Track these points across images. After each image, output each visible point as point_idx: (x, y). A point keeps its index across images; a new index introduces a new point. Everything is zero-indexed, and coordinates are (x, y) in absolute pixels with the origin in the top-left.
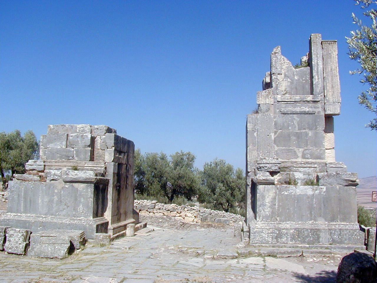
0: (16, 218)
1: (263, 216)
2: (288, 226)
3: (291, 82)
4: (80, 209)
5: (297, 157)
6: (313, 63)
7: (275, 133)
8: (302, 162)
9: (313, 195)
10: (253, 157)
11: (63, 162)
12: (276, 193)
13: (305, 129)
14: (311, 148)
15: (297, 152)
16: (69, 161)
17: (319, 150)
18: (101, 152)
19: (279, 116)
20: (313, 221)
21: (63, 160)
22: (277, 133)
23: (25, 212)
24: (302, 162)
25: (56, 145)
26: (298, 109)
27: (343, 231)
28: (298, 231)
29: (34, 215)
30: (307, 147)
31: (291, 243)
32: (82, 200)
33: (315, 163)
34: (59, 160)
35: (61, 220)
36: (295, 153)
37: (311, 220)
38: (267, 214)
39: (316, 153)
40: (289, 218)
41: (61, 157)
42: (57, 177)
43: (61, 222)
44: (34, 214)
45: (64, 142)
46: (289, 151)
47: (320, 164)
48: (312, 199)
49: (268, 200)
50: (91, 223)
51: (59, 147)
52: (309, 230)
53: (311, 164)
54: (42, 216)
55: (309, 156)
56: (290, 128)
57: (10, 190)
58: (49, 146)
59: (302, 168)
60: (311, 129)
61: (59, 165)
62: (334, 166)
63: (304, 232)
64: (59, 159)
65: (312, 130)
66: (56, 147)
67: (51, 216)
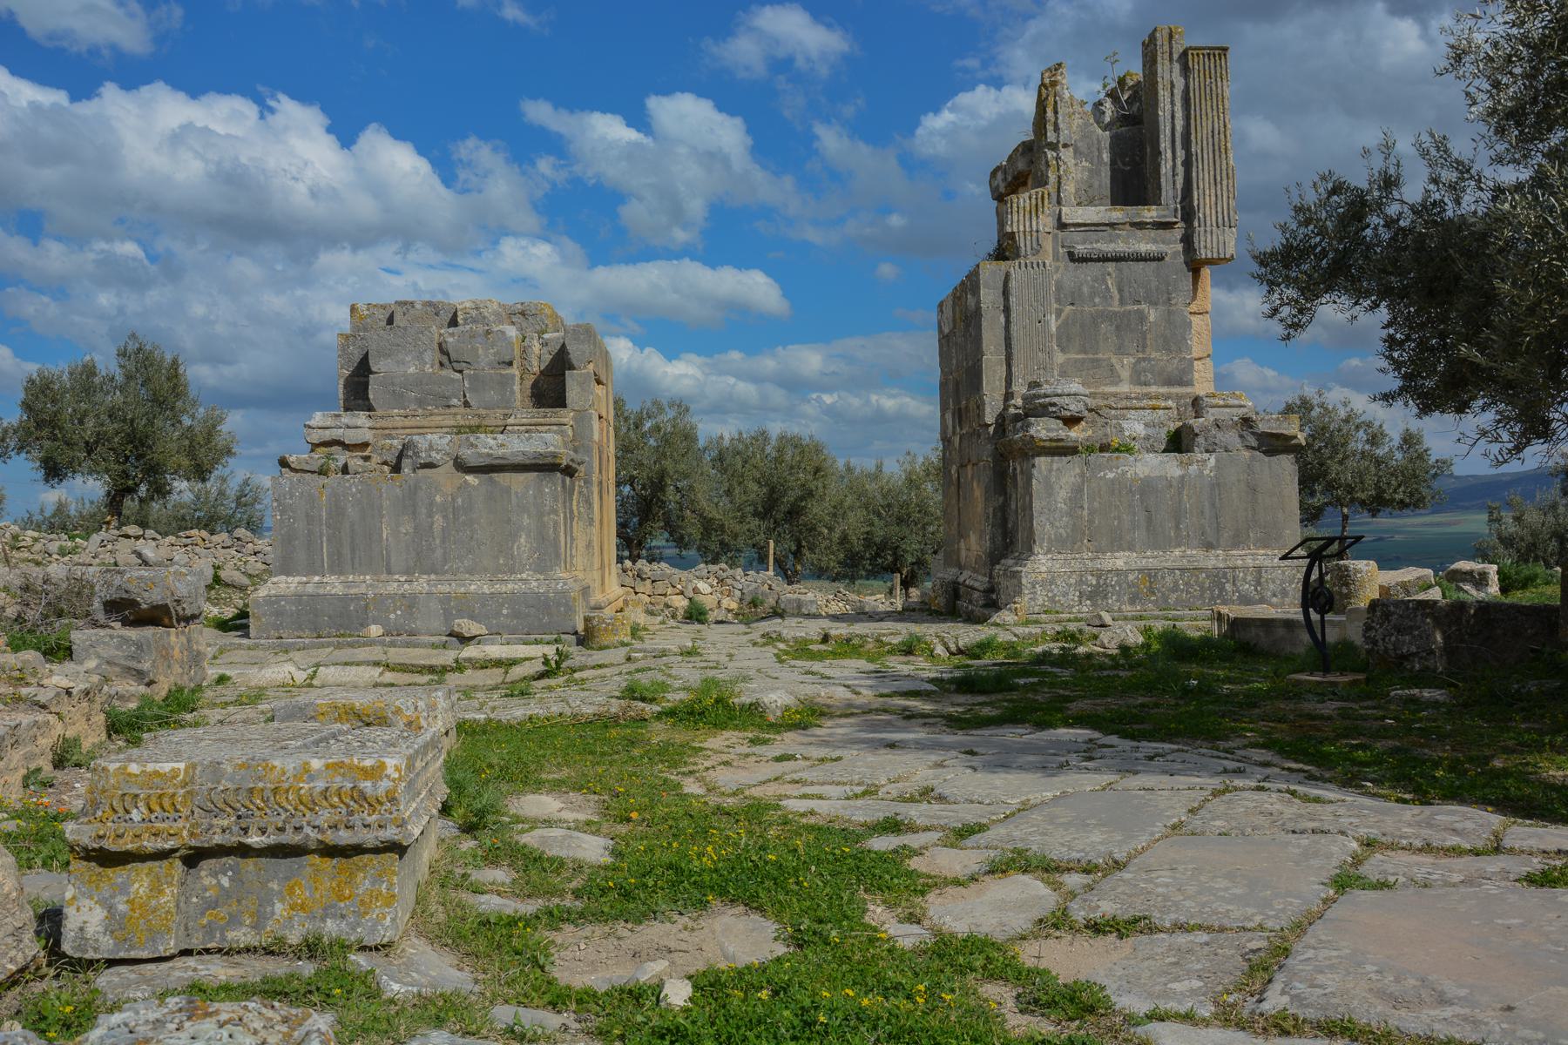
0: (310, 589)
1: (1049, 538)
2: (1120, 564)
3: (1090, 171)
4: (519, 548)
6: (1160, 113)
7: (1059, 313)
9: (1182, 477)
12: (1082, 475)
13: (1139, 302)
15: (1118, 367)
16: (448, 411)
17: (1176, 361)
22: (1063, 315)
23: (337, 568)
26: (1120, 247)
30: (1143, 352)
31: (1129, 608)
32: (526, 521)
33: (1167, 397)
35: (464, 585)
39: (1170, 369)
40: (1118, 543)
41: (421, 403)
43: (462, 590)
45: (429, 352)
46: (1096, 363)
47: (1179, 397)
49: (1062, 494)
50: (559, 587)
51: (412, 370)
53: (1157, 398)
54: (397, 577)
55: (1150, 376)
56: (1097, 300)
59: (1133, 412)
60: (1154, 303)
61: (419, 424)
62: (1221, 402)
63: (1163, 578)
65: (1156, 304)
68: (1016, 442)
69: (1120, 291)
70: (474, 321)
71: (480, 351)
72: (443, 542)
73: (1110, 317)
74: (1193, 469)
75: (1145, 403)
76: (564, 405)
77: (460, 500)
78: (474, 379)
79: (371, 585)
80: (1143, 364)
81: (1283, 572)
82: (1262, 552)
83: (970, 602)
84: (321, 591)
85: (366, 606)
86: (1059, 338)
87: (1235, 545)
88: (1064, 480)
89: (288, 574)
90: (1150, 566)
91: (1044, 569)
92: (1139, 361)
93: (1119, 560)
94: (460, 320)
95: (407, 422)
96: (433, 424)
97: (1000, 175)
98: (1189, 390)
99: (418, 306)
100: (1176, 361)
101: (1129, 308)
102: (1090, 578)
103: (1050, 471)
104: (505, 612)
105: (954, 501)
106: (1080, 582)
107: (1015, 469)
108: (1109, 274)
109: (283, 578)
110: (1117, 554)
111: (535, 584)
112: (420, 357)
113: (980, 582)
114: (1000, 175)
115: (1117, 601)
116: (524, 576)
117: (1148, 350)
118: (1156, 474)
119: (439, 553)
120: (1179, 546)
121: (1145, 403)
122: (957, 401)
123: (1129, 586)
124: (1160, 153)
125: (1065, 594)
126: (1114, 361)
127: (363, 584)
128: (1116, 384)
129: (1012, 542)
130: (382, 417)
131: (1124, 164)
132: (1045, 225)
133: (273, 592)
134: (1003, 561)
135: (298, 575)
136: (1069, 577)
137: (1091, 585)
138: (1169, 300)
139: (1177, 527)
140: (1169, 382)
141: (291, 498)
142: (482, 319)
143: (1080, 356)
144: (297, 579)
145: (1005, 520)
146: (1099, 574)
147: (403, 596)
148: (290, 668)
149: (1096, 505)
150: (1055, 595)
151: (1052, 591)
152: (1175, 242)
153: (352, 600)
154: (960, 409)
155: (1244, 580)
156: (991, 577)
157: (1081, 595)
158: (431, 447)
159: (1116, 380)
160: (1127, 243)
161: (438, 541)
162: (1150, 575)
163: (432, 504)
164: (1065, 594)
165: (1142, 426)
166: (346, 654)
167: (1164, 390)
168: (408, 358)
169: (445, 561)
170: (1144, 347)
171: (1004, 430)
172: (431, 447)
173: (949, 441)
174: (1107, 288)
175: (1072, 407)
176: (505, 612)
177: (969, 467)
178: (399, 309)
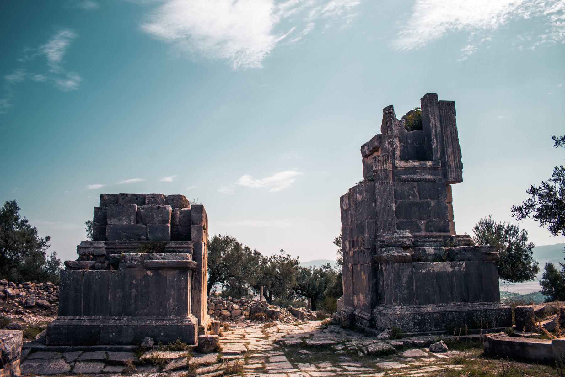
0: (74, 322)
2: (430, 309)
4: (169, 304)
5: (420, 230)
8: (426, 236)
9: (453, 271)
10: (372, 231)
11: (132, 243)
12: (412, 271)
13: (427, 199)
14: (434, 220)
17: (442, 222)
18: (180, 229)
19: (398, 184)
20: (455, 302)
21: (132, 240)
22: (397, 203)
23: (87, 313)
24: (426, 235)
25: (120, 220)
27: (489, 312)
28: (442, 315)
29: (101, 317)
30: (430, 218)
32: (173, 292)
33: (440, 237)
34: (125, 241)
35: (144, 321)
36: (417, 226)
37: (453, 301)
38: (404, 297)
39: (440, 226)
40: (428, 301)
42: (135, 263)
43: (143, 324)
44: (101, 316)
48: (451, 276)
51: (125, 223)
52: (453, 313)
55: (433, 228)
56: (411, 197)
57: (63, 284)
58: (111, 221)
63: (448, 315)
64: (126, 239)
66: (121, 222)
67: (127, 317)
68: (383, 257)
69: (419, 194)
70: (153, 203)
71: (155, 216)
72: (135, 301)
73: (416, 204)
74: (457, 268)
75: (431, 239)
76: (190, 240)
77: (144, 282)
79: (102, 321)
80: (430, 223)
81: (496, 312)
82: (486, 303)
83: (362, 324)
84: (79, 324)
85: (100, 330)
86: (396, 213)
87: (475, 300)
88: (405, 274)
89: (65, 315)
90: (442, 310)
91: (398, 313)
92: (428, 222)
93: (429, 308)
94: (146, 202)
95: (122, 246)
96: (133, 247)
97: (366, 148)
98: (448, 234)
99: (129, 196)
100: (442, 222)
101: (423, 200)
102: (418, 316)
103: (399, 269)
104: (162, 334)
105: (350, 278)
106: (414, 318)
107: (382, 268)
108: (415, 187)
109: (63, 317)
110: (428, 305)
111: (176, 321)
112: (129, 218)
113: (366, 316)
114: (366, 148)
115: (430, 326)
116: (171, 317)
117: (432, 217)
118: (442, 270)
119: (133, 306)
120: (453, 301)
121: (431, 239)
122: (352, 237)
123: (434, 320)
124: (431, 140)
125: (408, 324)
126: (418, 222)
127: (98, 321)
128: (420, 232)
129: (380, 299)
130: (111, 244)
131: (417, 144)
132: (389, 168)
133: (58, 323)
134: (377, 307)
135: (69, 315)
136: (410, 316)
137: (419, 319)
138: (439, 197)
139: (452, 292)
140: (440, 231)
141: (68, 281)
142: (155, 202)
143: (404, 220)
144: (69, 317)
145: (377, 289)
146: (421, 314)
147: (116, 326)
148: (62, 362)
149: (418, 284)
150: (404, 324)
151: (402, 322)
152: (439, 175)
153: (93, 328)
154: (353, 241)
155: (480, 315)
156: (372, 314)
157: (415, 324)
158: (132, 259)
159: (420, 230)
160: (421, 175)
161: (133, 301)
162: (442, 314)
163: (131, 284)
164: (408, 324)
165: (433, 250)
166: (88, 355)
167: (438, 234)
170: (430, 216)
171: (375, 252)
172: (132, 259)
173: (347, 253)
174: (414, 193)
175: (407, 243)
176: (162, 334)
177: (359, 266)
178: (121, 197)
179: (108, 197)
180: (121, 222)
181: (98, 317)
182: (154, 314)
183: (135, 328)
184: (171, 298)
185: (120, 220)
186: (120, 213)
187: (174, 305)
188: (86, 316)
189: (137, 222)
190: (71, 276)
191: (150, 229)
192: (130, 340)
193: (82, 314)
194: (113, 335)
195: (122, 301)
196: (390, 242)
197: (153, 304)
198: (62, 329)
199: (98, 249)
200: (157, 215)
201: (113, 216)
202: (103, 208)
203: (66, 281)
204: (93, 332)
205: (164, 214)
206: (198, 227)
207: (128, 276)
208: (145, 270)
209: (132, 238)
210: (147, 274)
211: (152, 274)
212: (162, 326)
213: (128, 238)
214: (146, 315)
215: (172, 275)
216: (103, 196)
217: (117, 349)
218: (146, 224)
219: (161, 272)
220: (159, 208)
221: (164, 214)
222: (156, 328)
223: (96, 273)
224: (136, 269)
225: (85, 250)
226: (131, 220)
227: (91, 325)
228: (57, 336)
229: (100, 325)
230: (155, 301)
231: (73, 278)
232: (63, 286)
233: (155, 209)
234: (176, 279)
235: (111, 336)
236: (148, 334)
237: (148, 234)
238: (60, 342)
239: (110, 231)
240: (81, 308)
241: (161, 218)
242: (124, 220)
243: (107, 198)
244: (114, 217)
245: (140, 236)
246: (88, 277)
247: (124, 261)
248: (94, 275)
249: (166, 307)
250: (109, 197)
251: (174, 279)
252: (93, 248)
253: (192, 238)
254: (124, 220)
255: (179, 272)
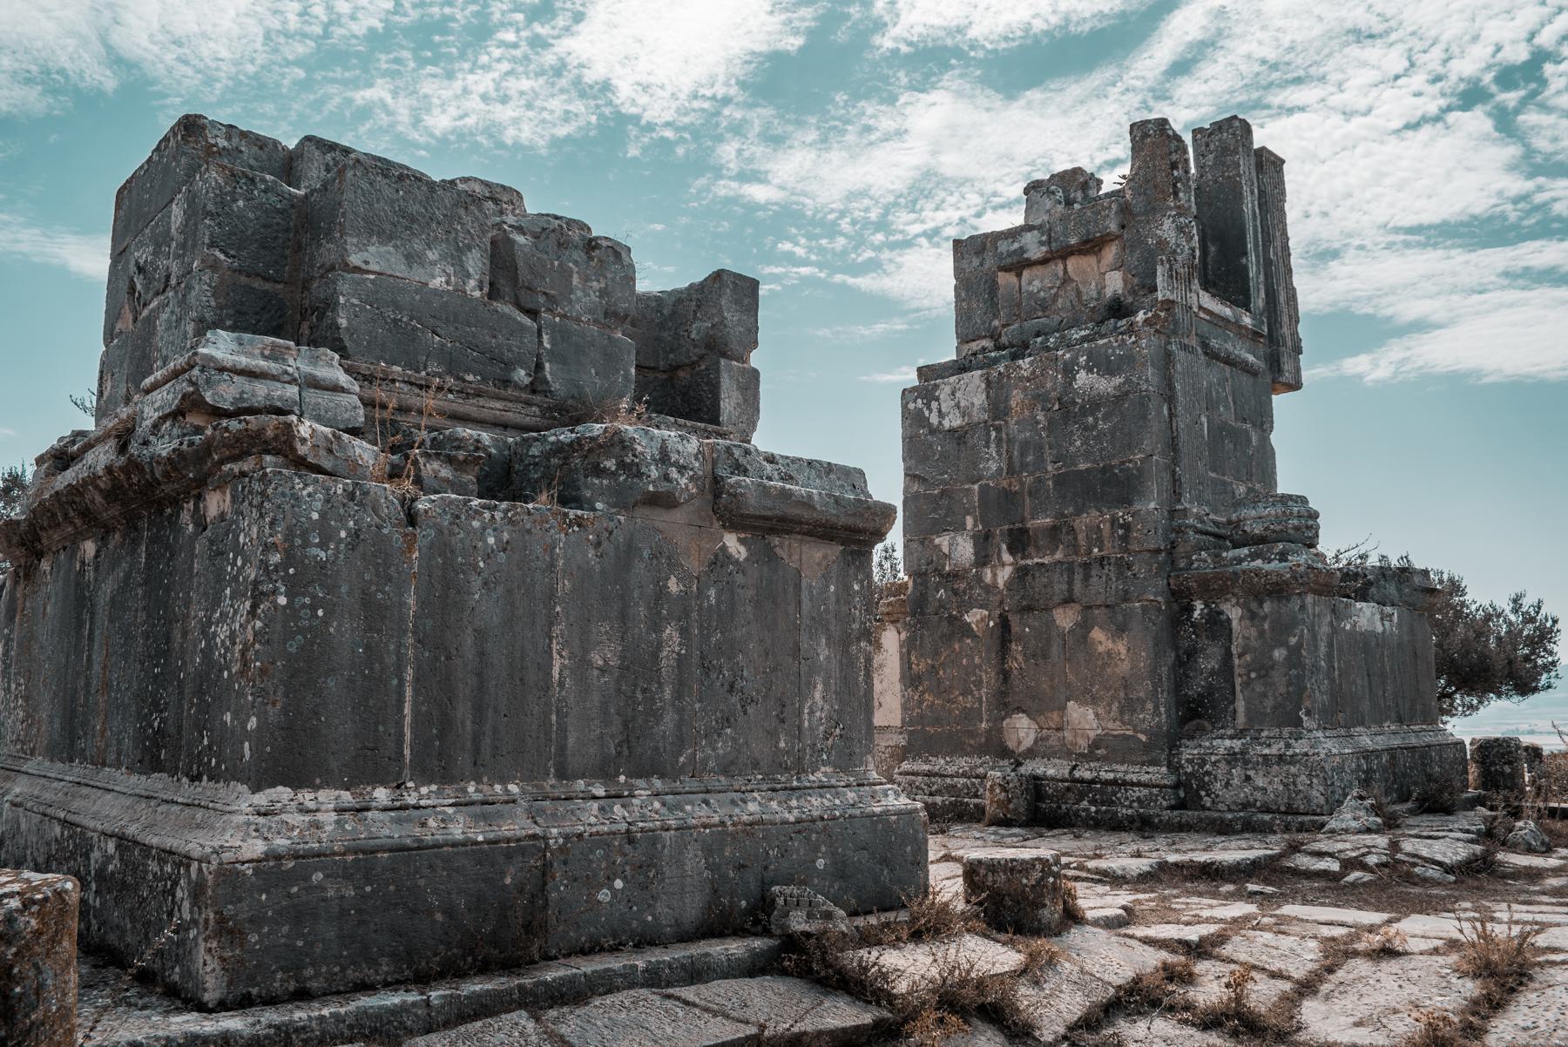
0: (384, 828)
44: (511, 779)
51: (438, 282)
57: (284, 565)
66: (418, 274)
71: (575, 280)
72: (678, 695)
78: (561, 334)
85: (545, 870)
109: (283, 793)
112: (456, 257)
119: (669, 720)
135: (326, 784)
141: (323, 545)
153: (509, 855)
161: (668, 692)
163: (661, 593)
168: (432, 255)
169: (680, 743)
172: (664, 457)
176: (820, 863)
179: (229, 138)
180: (418, 274)
181: (498, 788)
182: (756, 765)
183: (717, 840)
184: (819, 679)
185: (411, 259)
186: (413, 220)
187: (829, 718)
188: (430, 783)
189: (494, 293)
190: (342, 520)
191: (553, 341)
192: (692, 908)
193: (407, 772)
194: (614, 892)
195: (619, 691)
196: (1278, 528)
197: (750, 710)
198: (318, 877)
199: (327, 395)
200: (586, 279)
201: (377, 230)
202: (263, 180)
203: (306, 544)
204: (508, 881)
205: (613, 280)
206: (743, 375)
207: (646, 554)
208: (717, 524)
209: (468, 371)
210: (724, 548)
211: (742, 549)
212: (820, 824)
213: (453, 366)
214: (725, 771)
215: (819, 564)
216: (204, 127)
217: (683, 966)
218: (533, 313)
219: (781, 546)
220: (594, 248)
221: (613, 280)
222: (799, 832)
223: (487, 515)
224: (678, 516)
225: (247, 387)
226: (469, 276)
227: (496, 842)
228: (285, 929)
229: (545, 838)
230: (758, 692)
231: (355, 534)
232: (287, 579)
233: (576, 247)
234: (832, 588)
235: (604, 896)
236: (766, 868)
237: (547, 365)
238: (309, 972)
239: (363, 310)
240: (402, 735)
241: (601, 297)
242: (434, 263)
243: (222, 143)
244: (386, 237)
245: (509, 366)
246: (440, 532)
247: (621, 465)
248: (476, 524)
249: (800, 728)
250: (235, 140)
251: (828, 587)
252: (293, 381)
253: (724, 418)
254: (434, 263)
255: (842, 552)
